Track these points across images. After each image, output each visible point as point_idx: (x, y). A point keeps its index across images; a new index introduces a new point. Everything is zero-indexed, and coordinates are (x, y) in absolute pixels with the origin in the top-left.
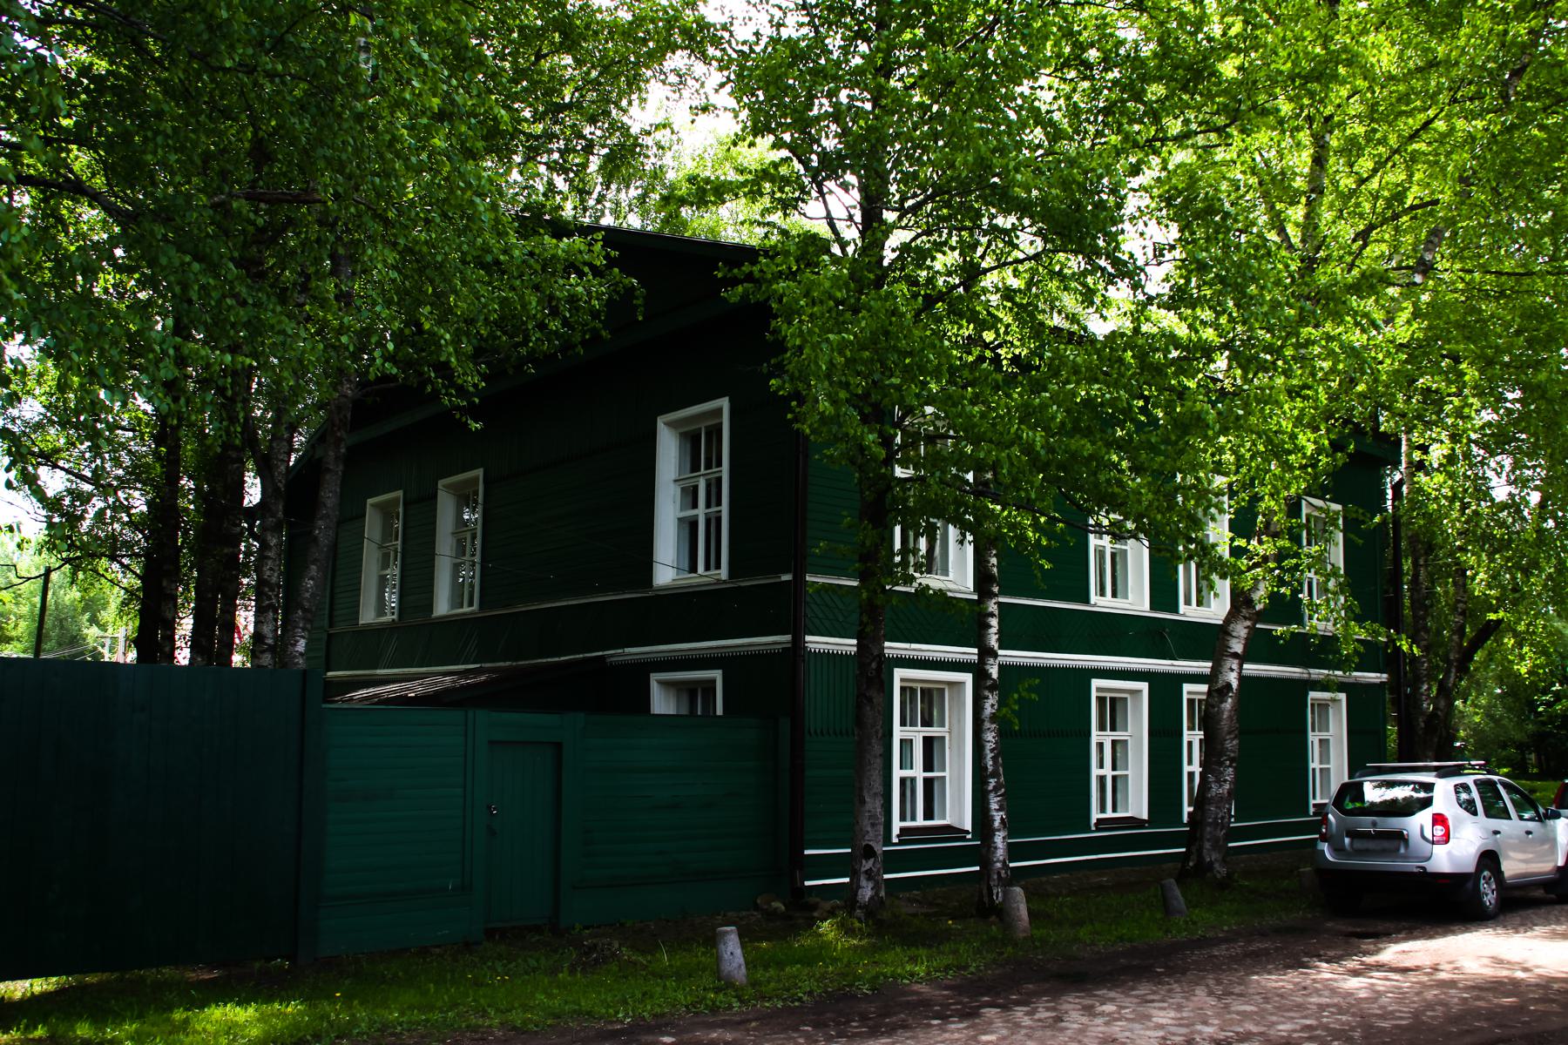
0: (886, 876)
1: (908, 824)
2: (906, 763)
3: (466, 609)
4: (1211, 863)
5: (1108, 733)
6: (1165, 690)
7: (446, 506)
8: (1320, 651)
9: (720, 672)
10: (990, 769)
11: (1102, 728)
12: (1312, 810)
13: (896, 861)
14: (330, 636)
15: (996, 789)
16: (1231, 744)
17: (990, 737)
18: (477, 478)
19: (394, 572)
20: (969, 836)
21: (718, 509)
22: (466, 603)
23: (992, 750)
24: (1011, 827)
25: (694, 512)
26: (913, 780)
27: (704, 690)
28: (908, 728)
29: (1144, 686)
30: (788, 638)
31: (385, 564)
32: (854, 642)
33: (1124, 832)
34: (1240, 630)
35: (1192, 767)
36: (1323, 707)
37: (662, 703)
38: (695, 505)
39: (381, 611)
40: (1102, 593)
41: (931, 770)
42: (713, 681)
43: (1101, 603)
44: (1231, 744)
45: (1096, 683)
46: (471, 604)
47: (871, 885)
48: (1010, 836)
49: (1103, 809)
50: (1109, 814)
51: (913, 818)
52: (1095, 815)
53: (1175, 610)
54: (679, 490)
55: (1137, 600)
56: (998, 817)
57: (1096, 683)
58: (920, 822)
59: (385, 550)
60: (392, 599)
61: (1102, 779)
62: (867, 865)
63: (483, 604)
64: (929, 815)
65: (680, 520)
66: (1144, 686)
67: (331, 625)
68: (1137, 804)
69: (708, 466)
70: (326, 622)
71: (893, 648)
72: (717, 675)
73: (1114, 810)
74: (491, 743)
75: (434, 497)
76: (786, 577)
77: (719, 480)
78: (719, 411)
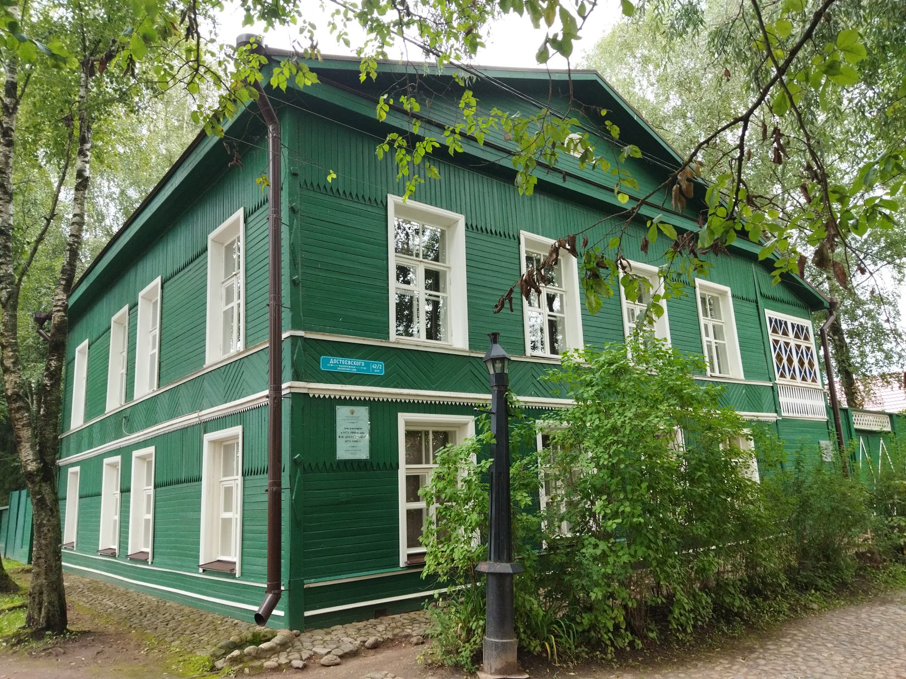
43: (395, 338)
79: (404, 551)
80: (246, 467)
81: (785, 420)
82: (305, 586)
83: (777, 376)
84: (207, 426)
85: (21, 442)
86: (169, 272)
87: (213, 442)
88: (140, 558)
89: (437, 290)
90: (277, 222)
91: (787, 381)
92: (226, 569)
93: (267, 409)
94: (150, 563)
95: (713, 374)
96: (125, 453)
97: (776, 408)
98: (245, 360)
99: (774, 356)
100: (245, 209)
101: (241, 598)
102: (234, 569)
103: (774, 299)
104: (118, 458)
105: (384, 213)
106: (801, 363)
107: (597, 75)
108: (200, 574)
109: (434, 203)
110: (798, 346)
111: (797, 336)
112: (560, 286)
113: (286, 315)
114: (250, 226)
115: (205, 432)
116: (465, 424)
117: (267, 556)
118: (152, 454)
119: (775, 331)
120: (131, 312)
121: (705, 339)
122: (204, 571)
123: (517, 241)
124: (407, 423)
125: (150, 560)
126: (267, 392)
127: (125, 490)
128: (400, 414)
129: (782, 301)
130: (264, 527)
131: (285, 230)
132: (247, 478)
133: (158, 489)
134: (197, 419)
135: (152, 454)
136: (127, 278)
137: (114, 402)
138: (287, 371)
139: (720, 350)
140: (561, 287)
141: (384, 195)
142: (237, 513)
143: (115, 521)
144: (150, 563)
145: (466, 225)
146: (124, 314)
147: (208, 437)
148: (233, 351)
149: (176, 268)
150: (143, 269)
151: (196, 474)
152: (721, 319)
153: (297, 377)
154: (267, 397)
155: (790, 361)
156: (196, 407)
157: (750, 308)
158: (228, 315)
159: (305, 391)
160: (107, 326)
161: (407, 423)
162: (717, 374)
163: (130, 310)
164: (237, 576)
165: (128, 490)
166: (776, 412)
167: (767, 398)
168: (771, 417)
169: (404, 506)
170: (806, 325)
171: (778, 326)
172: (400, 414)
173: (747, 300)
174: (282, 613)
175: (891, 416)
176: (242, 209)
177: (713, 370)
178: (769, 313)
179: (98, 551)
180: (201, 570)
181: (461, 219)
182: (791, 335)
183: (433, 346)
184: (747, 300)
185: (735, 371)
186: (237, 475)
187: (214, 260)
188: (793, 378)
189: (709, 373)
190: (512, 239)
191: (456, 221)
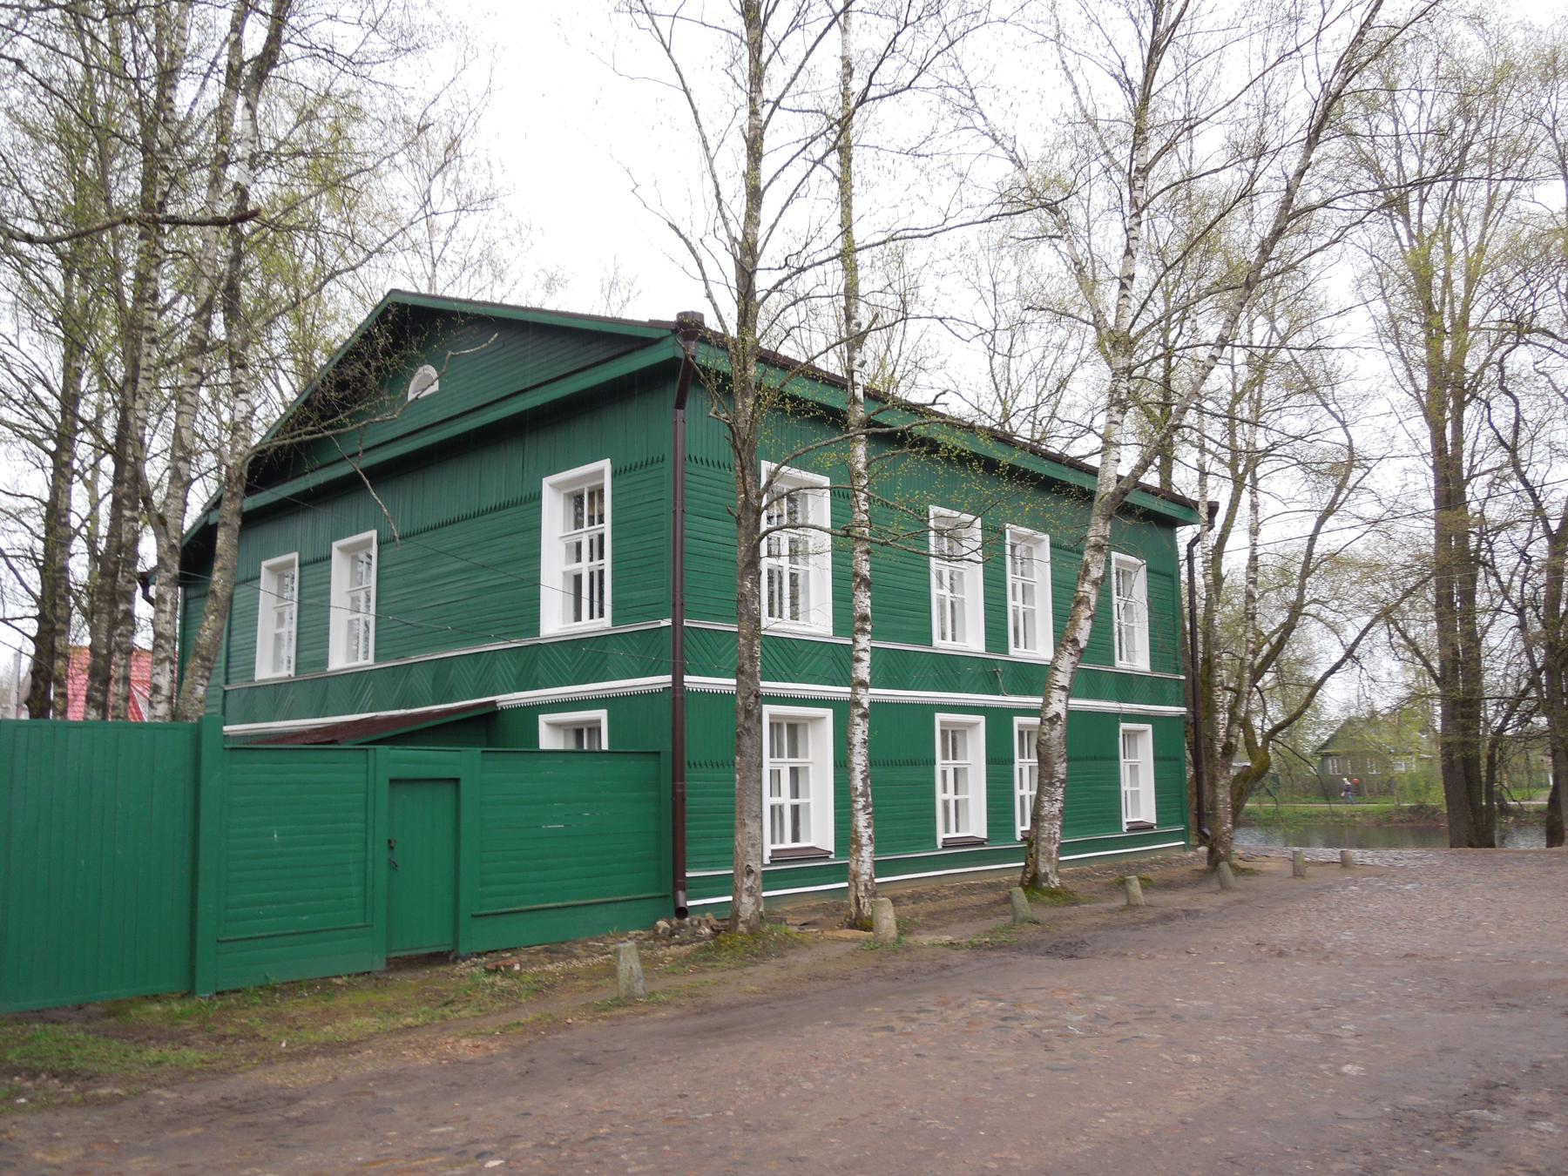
0: (765, 894)
1: (778, 846)
2: (776, 790)
3: (361, 662)
4: (1046, 874)
5: (951, 761)
6: (998, 721)
7: (339, 568)
8: (1127, 685)
9: (605, 711)
10: (860, 789)
11: (945, 757)
12: (1125, 827)
13: (770, 879)
14: (225, 692)
15: (865, 808)
16: (1061, 769)
17: (859, 760)
18: (370, 540)
19: (290, 628)
20: (832, 856)
21: (601, 562)
22: (361, 655)
23: (862, 772)
24: (879, 842)
25: (579, 565)
26: (781, 807)
27: (590, 730)
28: (776, 760)
29: (981, 719)
30: (669, 678)
31: (281, 619)
32: (734, 681)
33: (966, 851)
34: (1066, 663)
35: (1024, 791)
36: (1130, 735)
37: (548, 740)
38: (579, 560)
39: (277, 664)
40: (943, 638)
41: (797, 797)
42: (599, 721)
43: (941, 644)
44: (1061, 769)
45: (940, 717)
46: (366, 658)
47: (752, 900)
48: (877, 851)
49: (947, 830)
50: (953, 834)
51: (782, 841)
52: (941, 835)
53: (1006, 652)
54: (563, 548)
55: (973, 641)
56: (865, 832)
57: (940, 717)
58: (788, 844)
59: (281, 610)
60: (289, 651)
61: (946, 803)
62: (748, 882)
63: (377, 658)
64: (796, 838)
65: (564, 573)
66: (981, 719)
67: (227, 682)
68: (976, 825)
69: (591, 523)
70: (222, 680)
71: (767, 686)
72: (602, 715)
73: (957, 831)
74: (393, 781)
75: (537, 497)
76: (667, 622)
77: (601, 537)
78: (600, 473)
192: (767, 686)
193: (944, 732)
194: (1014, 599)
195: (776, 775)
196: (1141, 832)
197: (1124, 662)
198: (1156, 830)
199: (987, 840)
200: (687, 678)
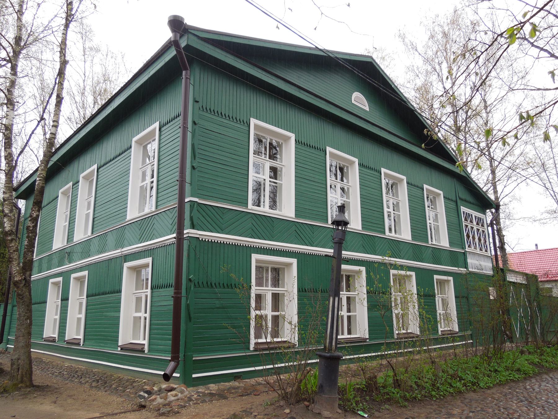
29: (294, 261)
36: (440, 282)
41: (350, 312)
43: (251, 207)
66: (294, 261)
68: (414, 328)
79: (253, 341)
80: (154, 283)
81: (471, 273)
82: (194, 359)
83: (467, 247)
84: (127, 258)
85: (13, 261)
86: (103, 162)
87: (130, 268)
88: (75, 342)
89: (276, 179)
90: (185, 129)
91: (472, 249)
92: (139, 348)
93: (170, 247)
94: (81, 345)
95: (432, 243)
96: (66, 275)
97: (466, 267)
98: (54, 254)
99: (465, 235)
100: (160, 122)
101: (148, 366)
102: (144, 348)
103: (466, 201)
104: (60, 279)
105: (247, 129)
106: (480, 240)
107: (372, 58)
108: (119, 351)
109: (277, 125)
110: (478, 230)
111: (478, 224)
112: (348, 182)
113: (188, 188)
114: (162, 133)
115: (125, 262)
116: (290, 265)
117: (171, 339)
118: (85, 276)
119: (466, 220)
120: (74, 187)
121: (428, 222)
122: (121, 349)
123: (324, 153)
124: (257, 261)
125: (82, 343)
126: (175, 235)
127: (65, 299)
128: (253, 255)
129: (470, 203)
130: (169, 321)
131: (189, 135)
132: (154, 290)
133: (89, 298)
134: (120, 254)
135: (85, 276)
136: (72, 166)
137: (80, 236)
138: (187, 222)
139: (437, 229)
140: (348, 183)
141: (248, 118)
142: (146, 313)
143: (55, 320)
144: (81, 345)
145: (296, 140)
146: (69, 188)
147: (126, 265)
148: (147, 210)
149: (108, 160)
150: (79, 163)
151: (117, 288)
152: (437, 210)
153: (193, 227)
154: (175, 238)
155: (474, 238)
156: (119, 244)
157: (453, 205)
158: (143, 189)
159: (198, 236)
160: (56, 196)
161: (257, 261)
162: (434, 243)
163: (73, 185)
164: (146, 352)
165: (67, 299)
166: (466, 268)
167: (461, 258)
168: (463, 270)
169: (253, 313)
170: (482, 218)
171: (468, 216)
172: (253, 255)
173: (452, 200)
174: (178, 375)
175: (526, 275)
176: (158, 123)
177: (432, 241)
178: (463, 209)
179: (43, 338)
180: (119, 349)
181: (293, 136)
182: (475, 223)
183: (274, 213)
184: (452, 200)
185: (444, 242)
186: (147, 288)
187: (135, 153)
188: (475, 248)
189: (430, 242)
190: (322, 152)
191: (289, 138)
192: (345, 254)
193: (437, 283)
194: (388, 207)
195: (259, 297)
196: (450, 336)
197: (393, 234)
198: (368, 342)
199: (458, 332)
200: (343, 252)
